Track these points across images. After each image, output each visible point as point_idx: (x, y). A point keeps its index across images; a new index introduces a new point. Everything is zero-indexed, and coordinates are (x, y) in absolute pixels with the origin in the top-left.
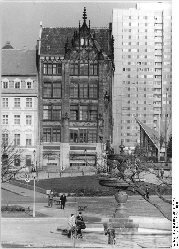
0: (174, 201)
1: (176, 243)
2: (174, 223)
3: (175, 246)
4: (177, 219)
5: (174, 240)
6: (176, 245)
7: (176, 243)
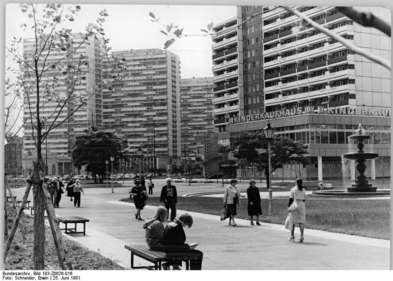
0: (59, 273)
1: (9, 276)
3: (5, 275)
4: (52, 278)
5: (14, 274)
6: (7, 276)
7: (9, 276)
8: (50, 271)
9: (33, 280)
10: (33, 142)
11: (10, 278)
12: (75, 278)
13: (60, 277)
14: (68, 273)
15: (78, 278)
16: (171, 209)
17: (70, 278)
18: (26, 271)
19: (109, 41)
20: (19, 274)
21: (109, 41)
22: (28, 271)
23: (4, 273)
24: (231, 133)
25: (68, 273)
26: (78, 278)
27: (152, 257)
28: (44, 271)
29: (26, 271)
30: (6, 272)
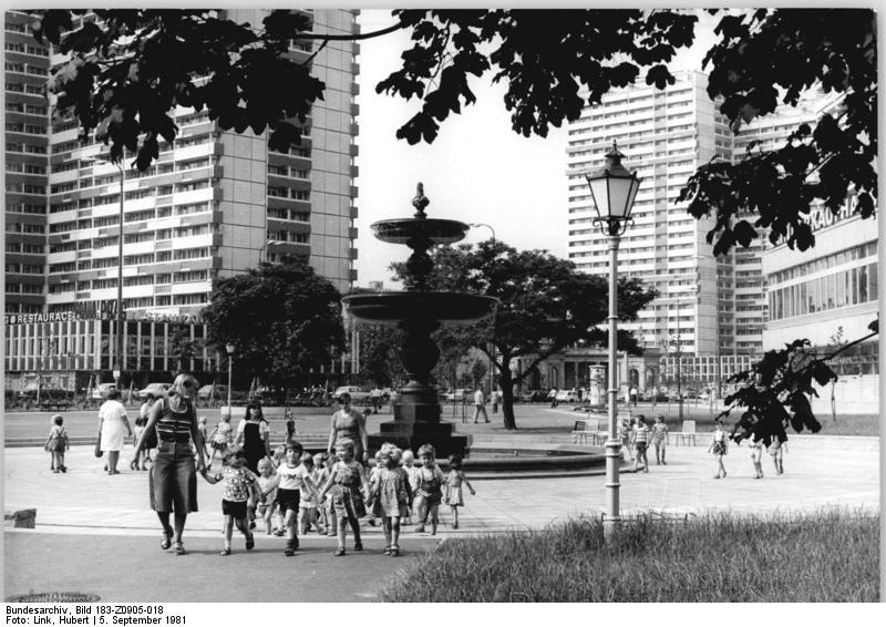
1: (22, 616)
2: (94, 611)
3: (11, 614)
5: (31, 611)
6: (16, 616)
7: (22, 616)
8: (113, 605)
9: (157, 625)
10: (445, 517)
11: (24, 621)
12: (175, 620)
13: (109, 618)
14: (153, 610)
15: (182, 620)
16: (472, 25)
17: (164, 621)
18: (58, 605)
19: (789, 105)
20: (43, 611)
21: (789, 105)
22: (64, 605)
23: (9, 610)
24: (721, 353)
25: (153, 610)
26: (182, 620)
27: (205, 539)
28: (100, 604)
29: (58, 605)
30: (15, 605)
